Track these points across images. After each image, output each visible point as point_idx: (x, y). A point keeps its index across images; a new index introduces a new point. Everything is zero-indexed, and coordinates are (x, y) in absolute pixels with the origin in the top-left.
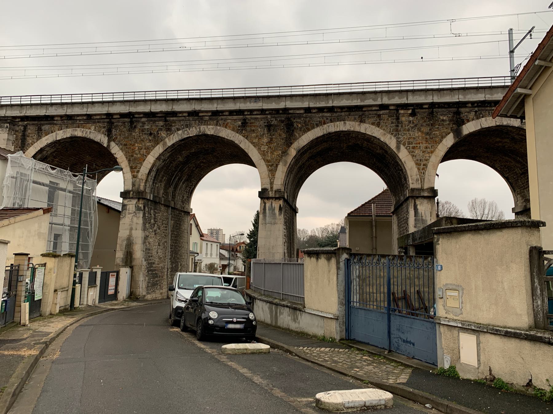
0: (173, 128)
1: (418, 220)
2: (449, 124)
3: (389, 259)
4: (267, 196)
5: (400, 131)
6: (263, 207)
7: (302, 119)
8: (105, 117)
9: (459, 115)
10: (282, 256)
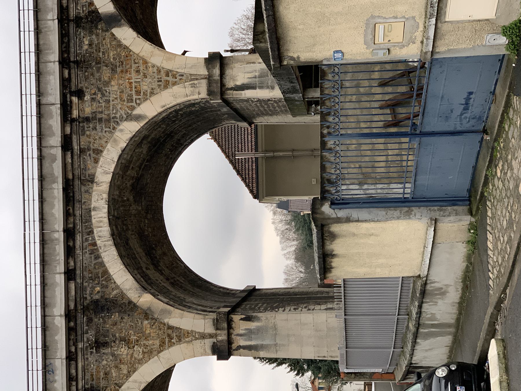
1: (262, 83)
2: (97, 35)
3: (329, 133)
4: (226, 344)
5: (109, 115)
6: (246, 351)
7: (85, 284)
9: (81, 18)
10: (332, 315)
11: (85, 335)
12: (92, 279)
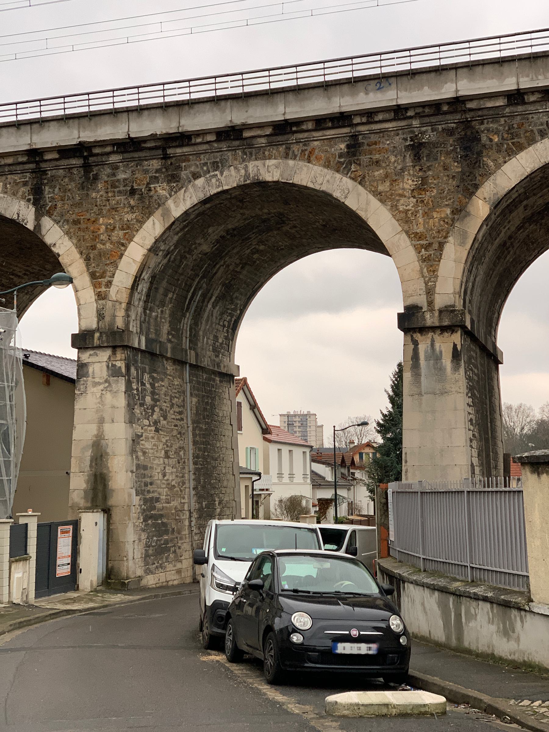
0: (184, 174)
4: (420, 325)
7: (502, 120)
8: (25, 159)
10: (466, 473)
11: (430, 128)
12: (509, 129)
